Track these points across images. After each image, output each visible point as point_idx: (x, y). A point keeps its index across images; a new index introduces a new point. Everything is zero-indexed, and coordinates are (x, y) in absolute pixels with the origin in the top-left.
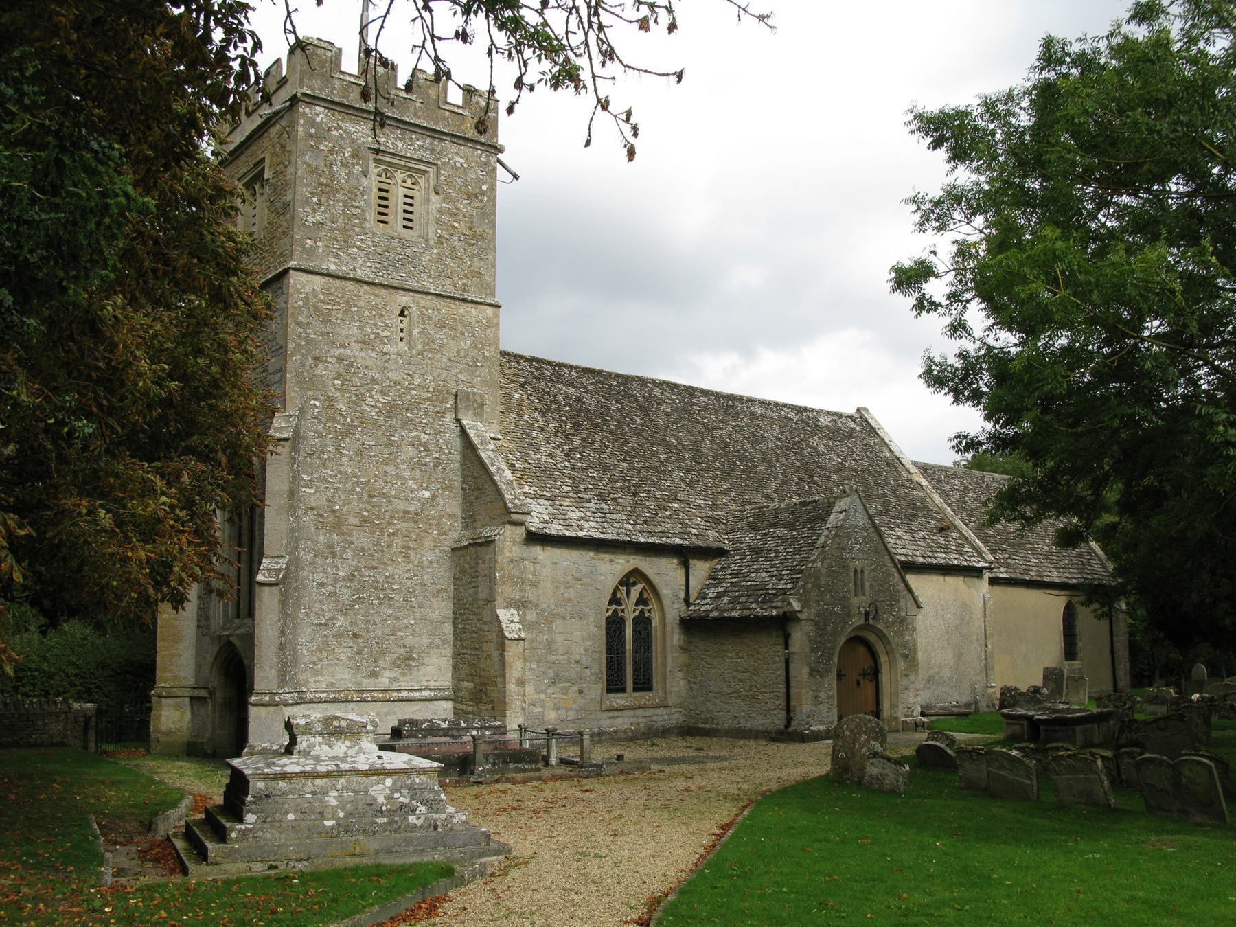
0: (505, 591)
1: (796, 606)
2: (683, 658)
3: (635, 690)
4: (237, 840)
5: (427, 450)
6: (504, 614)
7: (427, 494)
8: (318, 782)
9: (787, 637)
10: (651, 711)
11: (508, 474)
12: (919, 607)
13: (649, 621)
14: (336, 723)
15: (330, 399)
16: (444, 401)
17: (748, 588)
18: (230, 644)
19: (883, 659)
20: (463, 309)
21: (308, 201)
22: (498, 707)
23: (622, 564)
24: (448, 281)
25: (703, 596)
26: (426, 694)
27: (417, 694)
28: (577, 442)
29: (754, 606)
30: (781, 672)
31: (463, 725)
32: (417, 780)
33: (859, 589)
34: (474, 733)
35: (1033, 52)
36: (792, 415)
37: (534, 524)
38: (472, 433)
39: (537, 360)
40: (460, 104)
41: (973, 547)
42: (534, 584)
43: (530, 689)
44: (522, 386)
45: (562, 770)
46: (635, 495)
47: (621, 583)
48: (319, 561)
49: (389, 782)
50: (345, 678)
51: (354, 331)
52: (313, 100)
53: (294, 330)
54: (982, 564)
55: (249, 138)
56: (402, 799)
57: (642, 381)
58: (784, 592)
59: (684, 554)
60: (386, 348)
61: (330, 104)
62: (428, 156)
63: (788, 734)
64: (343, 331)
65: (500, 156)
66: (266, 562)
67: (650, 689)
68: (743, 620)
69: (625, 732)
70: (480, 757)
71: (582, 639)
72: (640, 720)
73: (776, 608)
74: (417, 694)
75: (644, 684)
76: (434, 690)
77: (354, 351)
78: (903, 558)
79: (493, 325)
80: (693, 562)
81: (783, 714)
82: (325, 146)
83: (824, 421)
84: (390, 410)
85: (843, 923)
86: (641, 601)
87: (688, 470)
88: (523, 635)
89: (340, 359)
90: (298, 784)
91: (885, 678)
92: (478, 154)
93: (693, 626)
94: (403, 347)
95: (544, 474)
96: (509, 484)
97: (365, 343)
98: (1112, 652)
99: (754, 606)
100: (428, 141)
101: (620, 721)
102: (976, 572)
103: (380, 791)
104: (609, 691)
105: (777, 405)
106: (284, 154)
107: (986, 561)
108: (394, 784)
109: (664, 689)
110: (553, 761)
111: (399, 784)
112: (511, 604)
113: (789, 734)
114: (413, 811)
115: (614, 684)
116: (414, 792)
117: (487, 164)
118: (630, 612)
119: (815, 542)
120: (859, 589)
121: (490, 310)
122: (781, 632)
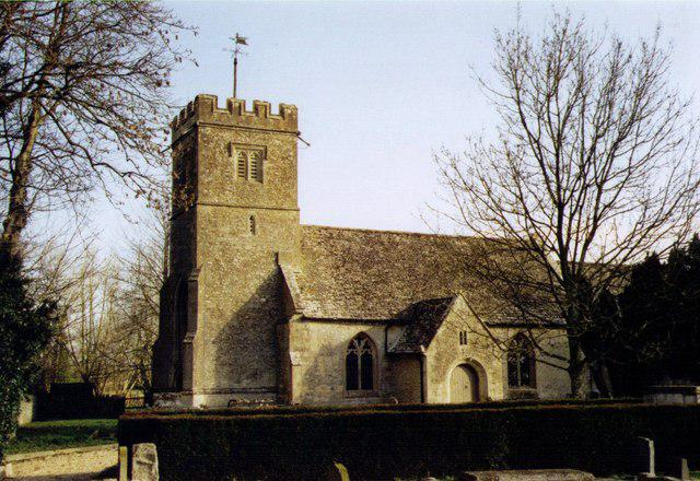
6: (293, 354)
19: (480, 375)
20: (282, 213)
42: (307, 340)
48: (525, 175)
53: (199, 231)
61: (214, 125)
64: (222, 229)
82: (212, 145)
85: (697, 130)
86: (367, 346)
89: (221, 243)
92: (288, 137)
97: (233, 234)
112: (296, 350)
115: (351, 384)
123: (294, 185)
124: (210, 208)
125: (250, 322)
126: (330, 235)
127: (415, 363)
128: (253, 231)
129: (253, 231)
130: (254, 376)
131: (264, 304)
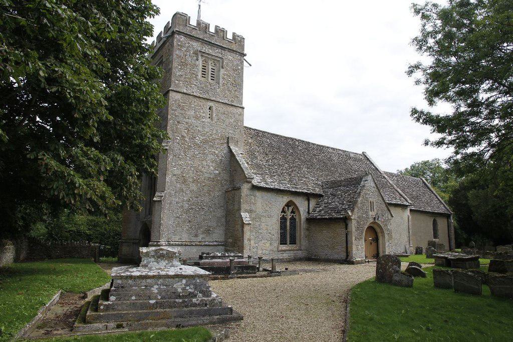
0: (244, 206)
2: (307, 233)
3: (290, 244)
4: (103, 311)
5: (217, 156)
6: (244, 215)
7: (217, 172)
8: (149, 281)
10: (295, 252)
11: (246, 165)
12: (392, 216)
13: (295, 219)
14: (161, 252)
15: (183, 136)
17: (331, 208)
18: (146, 224)
19: (380, 235)
21: (177, 67)
22: (241, 249)
23: (286, 199)
24: (226, 99)
25: (314, 211)
26: (215, 243)
27: (211, 243)
28: (270, 157)
29: (334, 214)
30: (344, 238)
31: (227, 255)
32: (198, 281)
33: (372, 209)
34: (231, 258)
38: (233, 151)
39: (257, 130)
40: (231, 39)
41: (404, 198)
43: (252, 242)
44: (251, 138)
45: (265, 273)
46: (290, 175)
47: (286, 205)
49: (184, 281)
51: (193, 113)
52: (180, 33)
54: (407, 204)
55: (159, 49)
56: (190, 290)
58: (345, 209)
59: (308, 196)
60: (203, 120)
61: (186, 35)
62: (220, 55)
63: (347, 260)
65: (245, 57)
67: (295, 243)
68: (330, 219)
69: (286, 259)
70: (232, 267)
71: (272, 226)
72: (292, 255)
73: (342, 215)
74: (211, 243)
75: (293, 242)
76: (218, 242)
77: (193, 121)
78: (486, 154)
79: (242, 115)
81: (345, 254)
84: (205, 142)
86: (293, 212)
88: (250, 222)
90: (138, 281)
91: (380, 241)
92: (238, 57)
94: (209, 120)
95: (258, 167)
96: (247, 168)
98: (449, 236)
99: (334, 214)
100: (220, 50)
101: (284, 255)
102: (404, 207)
103: (179, 286)
104: (281, 244)
105: (337, 149)
106: (170, 53)
107: (409, 203)
108: (186, 282)
109: (300, 244)
110: (261, 269)
111: (189, 282)
112: (246, 211)
113: (348, 261)
115: (283, 241)
117: (240, 60)
119: (355, 192)
120: (372, 209)
121: (240, 110)
122: (344, 224)
124: (178, 96)
125: (206, 189)
126: (258, 135)
127: (342, 225)
128: (211, 118)
129: (211, 118)
130: (208, 232)
131: (216, 175)
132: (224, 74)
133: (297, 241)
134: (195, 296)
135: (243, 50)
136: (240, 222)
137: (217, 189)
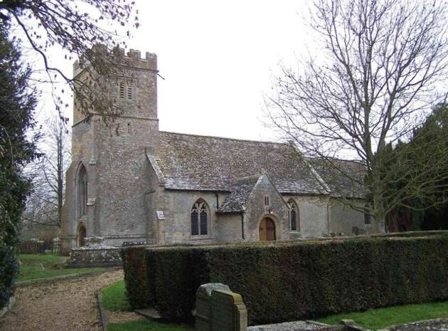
1: (244, 208)
5: (137, 165)
9: (243, 217)
15: (107, 152)
16: (142, 150)
19: (276, 224)
23: (196, 197)
28: (185, 160)
35: (67, 117)
36: (264, 145)
37: (168, 186)
42: (168, 203)
44: (169, 143)
50: (114, 232)
57: (211, 138)
59: (216, 193)
66: (89, 200)
75: (204, 232)
80: (219, 195)
83: (275, 146)
84: (125, 154)
86: (203, 207)
87: (221, 166)
92: (151, 74)
93: (219, 214)
94: (129, 135)
95: (172, 170)
96: (160, 174)
112: (160, 210)
114: (111, 258)
115: (194, 232)
116: (113, 255)
118: (199, 211)
120: (267, 203)
121: (156, 122)
123: (155, 103)
126: (175, 138)
127: (240, 217)
131: (137, 181)
132: (140, 93)
133: (208, 232)
134: (111, 258)
135: (156, 67)
136: (156, 219)
137: (137, 192)
